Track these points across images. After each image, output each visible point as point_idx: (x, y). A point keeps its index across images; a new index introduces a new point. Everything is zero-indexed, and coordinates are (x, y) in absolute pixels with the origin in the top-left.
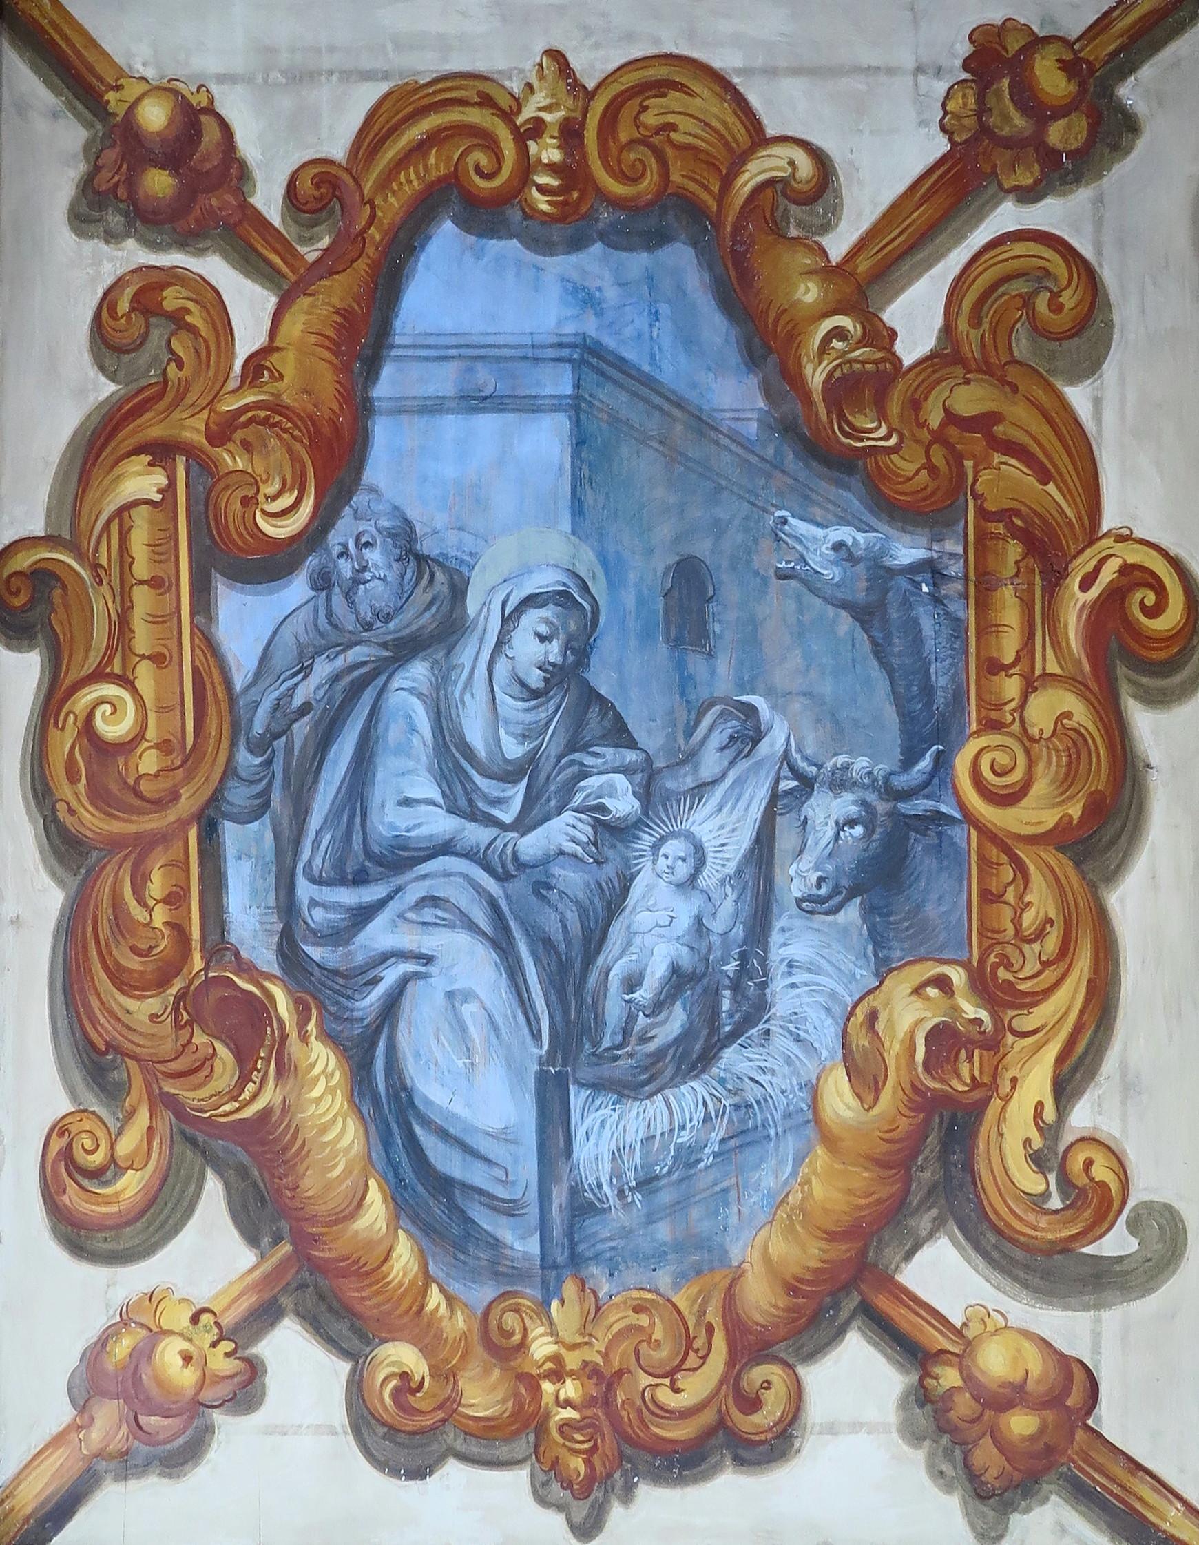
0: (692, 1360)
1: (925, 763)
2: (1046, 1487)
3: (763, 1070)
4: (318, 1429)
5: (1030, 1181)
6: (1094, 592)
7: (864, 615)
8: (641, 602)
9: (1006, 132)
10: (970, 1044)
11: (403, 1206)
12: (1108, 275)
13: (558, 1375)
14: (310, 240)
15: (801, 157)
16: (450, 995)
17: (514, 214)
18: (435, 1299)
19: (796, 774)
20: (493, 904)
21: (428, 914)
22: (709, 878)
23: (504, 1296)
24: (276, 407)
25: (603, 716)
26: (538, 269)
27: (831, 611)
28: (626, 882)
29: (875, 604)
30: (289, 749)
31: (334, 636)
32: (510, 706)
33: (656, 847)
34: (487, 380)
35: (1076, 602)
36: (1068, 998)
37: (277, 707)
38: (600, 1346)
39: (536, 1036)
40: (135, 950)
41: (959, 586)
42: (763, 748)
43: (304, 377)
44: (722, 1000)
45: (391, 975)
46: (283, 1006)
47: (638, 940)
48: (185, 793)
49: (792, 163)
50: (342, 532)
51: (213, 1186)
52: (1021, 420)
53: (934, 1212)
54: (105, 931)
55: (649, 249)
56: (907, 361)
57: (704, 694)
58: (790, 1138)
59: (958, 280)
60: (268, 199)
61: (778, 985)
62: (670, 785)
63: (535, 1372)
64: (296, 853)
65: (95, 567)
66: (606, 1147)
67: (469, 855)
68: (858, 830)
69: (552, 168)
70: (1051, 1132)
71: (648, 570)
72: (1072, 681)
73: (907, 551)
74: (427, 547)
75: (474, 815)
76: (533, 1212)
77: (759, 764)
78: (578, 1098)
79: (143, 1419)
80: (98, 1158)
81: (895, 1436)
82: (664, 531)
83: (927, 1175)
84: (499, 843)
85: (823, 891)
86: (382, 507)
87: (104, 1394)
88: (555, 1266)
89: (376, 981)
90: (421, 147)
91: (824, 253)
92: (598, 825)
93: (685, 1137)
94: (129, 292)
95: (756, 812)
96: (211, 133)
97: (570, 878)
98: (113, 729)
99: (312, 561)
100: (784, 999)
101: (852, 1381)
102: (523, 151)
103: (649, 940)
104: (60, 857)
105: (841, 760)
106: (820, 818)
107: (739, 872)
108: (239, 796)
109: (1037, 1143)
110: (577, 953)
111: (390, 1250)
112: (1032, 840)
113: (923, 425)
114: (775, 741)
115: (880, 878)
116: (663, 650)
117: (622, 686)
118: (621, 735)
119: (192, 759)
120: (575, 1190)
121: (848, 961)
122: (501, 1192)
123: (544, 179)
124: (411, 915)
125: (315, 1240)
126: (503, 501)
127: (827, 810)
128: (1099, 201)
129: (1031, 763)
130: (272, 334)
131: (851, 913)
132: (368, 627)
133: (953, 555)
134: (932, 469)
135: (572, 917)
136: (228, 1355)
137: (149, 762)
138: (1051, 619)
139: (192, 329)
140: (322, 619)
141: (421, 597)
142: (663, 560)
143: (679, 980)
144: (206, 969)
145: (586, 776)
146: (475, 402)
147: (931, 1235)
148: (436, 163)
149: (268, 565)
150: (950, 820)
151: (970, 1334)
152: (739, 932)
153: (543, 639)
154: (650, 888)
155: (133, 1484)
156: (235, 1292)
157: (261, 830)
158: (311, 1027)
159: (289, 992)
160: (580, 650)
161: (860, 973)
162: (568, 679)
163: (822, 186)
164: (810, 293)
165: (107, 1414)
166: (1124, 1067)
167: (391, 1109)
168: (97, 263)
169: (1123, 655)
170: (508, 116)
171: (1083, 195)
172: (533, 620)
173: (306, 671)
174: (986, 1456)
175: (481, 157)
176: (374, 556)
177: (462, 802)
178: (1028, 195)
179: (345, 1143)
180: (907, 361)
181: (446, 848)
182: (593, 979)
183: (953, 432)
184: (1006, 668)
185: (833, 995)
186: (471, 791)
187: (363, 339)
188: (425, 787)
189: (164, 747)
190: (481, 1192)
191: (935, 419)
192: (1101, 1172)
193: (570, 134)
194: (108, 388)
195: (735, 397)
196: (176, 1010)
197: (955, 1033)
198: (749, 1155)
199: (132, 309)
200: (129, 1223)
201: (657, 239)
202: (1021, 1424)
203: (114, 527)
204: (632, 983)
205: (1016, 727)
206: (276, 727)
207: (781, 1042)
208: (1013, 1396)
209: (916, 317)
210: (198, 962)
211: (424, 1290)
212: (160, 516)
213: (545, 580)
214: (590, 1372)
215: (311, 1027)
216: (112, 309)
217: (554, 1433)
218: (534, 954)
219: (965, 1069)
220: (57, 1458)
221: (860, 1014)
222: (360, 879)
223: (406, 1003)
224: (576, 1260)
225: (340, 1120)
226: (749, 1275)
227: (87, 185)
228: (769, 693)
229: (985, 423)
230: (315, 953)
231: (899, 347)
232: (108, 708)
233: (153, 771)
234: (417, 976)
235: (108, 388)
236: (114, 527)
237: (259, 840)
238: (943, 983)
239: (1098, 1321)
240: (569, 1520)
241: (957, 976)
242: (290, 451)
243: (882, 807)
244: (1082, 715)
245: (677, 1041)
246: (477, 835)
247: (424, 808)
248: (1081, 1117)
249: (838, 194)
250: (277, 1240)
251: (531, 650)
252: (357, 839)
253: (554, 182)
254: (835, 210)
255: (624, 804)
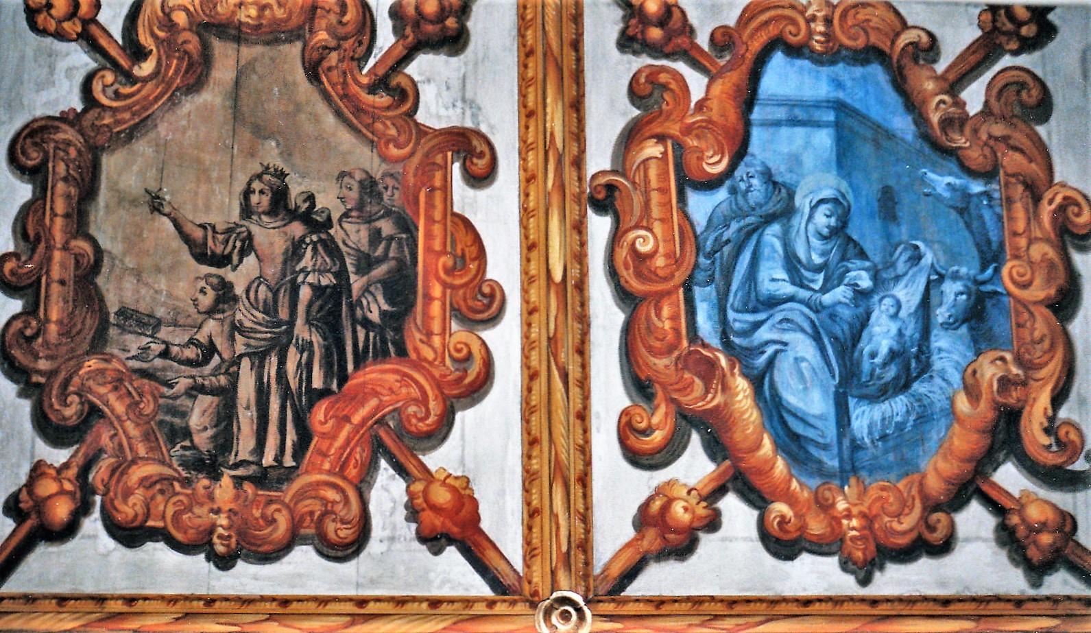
0: (907, 510)
1: (990, 271)
2: (1058, 565)
3: (930, 392)
4: (745, 539)
5: (1045, 440)
6: (1053, 206)
7: (962, 212)
8: (868, 203)
9: (1004, 29)
10: (1016, 384)
11: (778, 446)
12: (1050, 85)
13: (849, 516)
14: (721, 57)
15: (923, 34)
16: (796, 359)
17: (806, 51)
18: (795, 485)
19: (937, 273)
20: (812, 322)
21: (785, 326)
22: (903, 314)
23: (824, 484)
24: (710, 121)
25: (855, 247)
26: (818, 72)
27: (947, 210)
28: (868, 315)
29: (964, 206)
30: (721, 258)
31: (739, 212)
32: (816, 242)
33: (881, 300)
34: (800, 114)
35: (1046, 211)
36: (1053, 368)
37: (716, 240)
38: (866, 504)
39: (833, 377)
40: (657, 339)
41: (999, 202)
42: (923, 261)
43: (724, 111)
44: (911, 364)
45: (770, 350)
46: (723, 361)
47: (874, 339)
48: (677, 274)
49: (919, 36)
50: (740, 172)
51: (695, 438)
52: (1019, 138)
53: (1005, 452)
54: (643, 331)
55: (862, 65)
56: (971, 114)
57: (896, 240)
58: (943, 420)
59: (989, 84)
60: (703, 40)
61: (935, 357)
62: (885, 275)
63: (839, 515)
64: (727, 301)
65: (634, 183)
66: (865, 423)
67: (801, 302)
68: (964, 297)
69: (821, 33)
70: (1052, 419)
71: (870, 190)
72: (1047, 240)
73: (977, 187)
74: (779, 179)
75: (802, 286)
76: (835, 450)
77: (920, 270)
78: (852, 402)
79: (667, 536)
80: (643, 425)
81: (993, 544)
82: (875, 176)
83: (1001, 436)
84: (814, 298)
85: (951, 320)
86: (757, 162)
87: (650, 525)
88: (845, 471)
89: (763, 353)
90: (766, 23)
91: (935, 71)
92: (855, 291)
93: (899, 419)
94: (644, 75)
95: (922, 287)
96: (677, 14)
97: (846, 313)
98: (644, 248)
99: (728, 183)
100: (937, 365)
101: (974, 520)
102: (809, 27)
103: (879, 338)
104: (622, 300)
105: (955, 268)
106: (948, 291)
107: (916, 311)
108: (700, 276)
109: (1046, 424)
110: (849, 344)
111: (774, 464)
112: (1036, 303)
113: (979, 139)
114: (928, 258)
115: (977, 315)
116: (878, 223)
117: (1045, 74)
118: (862, 255)
119: (678, 262)
120: (853, 440)
121: (962, 348)
122: (821, 440)
123: (818, 38)
124: (779, 326)
125: (742, 459)
126: (808, 161)
127: (951, 289)
128: (1043, 57)
129: (1033, 273)
130: (708, 91)
131: (964, 330)
132: (754, 209)
133: (995, 190)
134: (985, 156)
135: (846, 327)
136: (704, 508)
137: (660, 262)
138: (1037, 215)
139: (672, 90)
140: (734, 207)
141: (775, 199)
142: (876, 187)
143: (893, 355)
144: (689, 346)
145: (848, 271)
146: (794, 122)
147: (1004, 462)
148: (773, 30)
149: (711, 184)
150: (1001, 294)
151: (1023, 501)
152: (917, 336)
153: (828, 216)
154: (878, 318)
155: (663, 564)
156: (706, 481)
157: (710, 290)
158: (736, 371)
159: (726, 356)
160: (844, 222)
161: (968, 354)
162: (839, 232)
163: (932, 48)
164: (930, 86)
165: (651, 533)
166: (1079, 394)
167: (773, 407)
168: (629, 63)
169: (1067, 235)
170: (802, 13)
171: (1037, 55)
172: (824, 209)
173: (728, 226)
174: (1034, 554)
175: (791, 28)
176: (755, 182)
177: (797, 280)
178: (1015, 53)
179: (752, 419)
180: (971, 114)
181: (791, 299)
182: (856, 354)
183: (992, 142)
184: (1020, 235)
185: (957, 362)
186: (801, 277)
187: (748, 97)
188: (782, 274)
189: (667, 256)
190: (812, 440)
191: (984, 137)
192: (1073, 436)
193: (828, 21)
194: (636, 112)
195: (902, 124)
196: (676, 364)
197: (1009, 380)
198: (927, 427)
199: (646, 82)
200: (659, 452)
201: (865, 62)
202: (1046, 539)
203: (642, 167)
204: (873, 355)
205: (1025, 258)
206: (715, 248)
207: (938, 381)
208: (1043, 527)
209: (974, 96)
210: (685, 343)
211: (790, 481)
212: (660, 163)
213: (827, 193)
214: (863, 515)
215: (736, 371)
216: (637, 81)
217: (849, 543)
218: (831, 343)
219: (1014, 394)
220: (628, 554)
221: (970, 371)
222: (755, 311)
223: (777, 363)
224: (855, 470)
225: (750, 411)
226: (929, 476)
227: (623, 33)
228: (925, 241)
229: (1005, 139)
230: (737, 340)
231: (967, 108)
232: (641, 240)
233: (662, 265)
234: (782, 351)
235: (636, 112)
236: (642, 167)
237: (710, 294)
238: (1002, 359)
239: (1074, 498)
240: (857, 578)
241: (1008, 356)
242: (716, 139)
243: (973, 288)
244: (1051, 253)
245: (894, 379)
246: (804, 294)
247: (780, 283)
248: (1063, 413)
249: (938, 48)
250: (724, 459)
251: (822, 220)
252: (753, 295)
253: (822, 39)
254: (938, 54)
255: (865, 282)
